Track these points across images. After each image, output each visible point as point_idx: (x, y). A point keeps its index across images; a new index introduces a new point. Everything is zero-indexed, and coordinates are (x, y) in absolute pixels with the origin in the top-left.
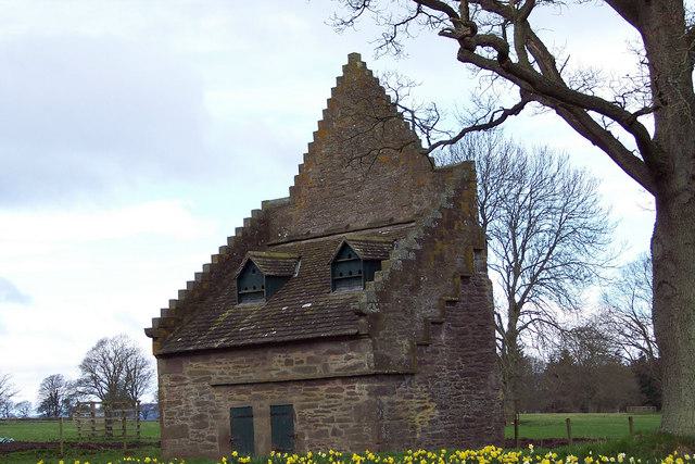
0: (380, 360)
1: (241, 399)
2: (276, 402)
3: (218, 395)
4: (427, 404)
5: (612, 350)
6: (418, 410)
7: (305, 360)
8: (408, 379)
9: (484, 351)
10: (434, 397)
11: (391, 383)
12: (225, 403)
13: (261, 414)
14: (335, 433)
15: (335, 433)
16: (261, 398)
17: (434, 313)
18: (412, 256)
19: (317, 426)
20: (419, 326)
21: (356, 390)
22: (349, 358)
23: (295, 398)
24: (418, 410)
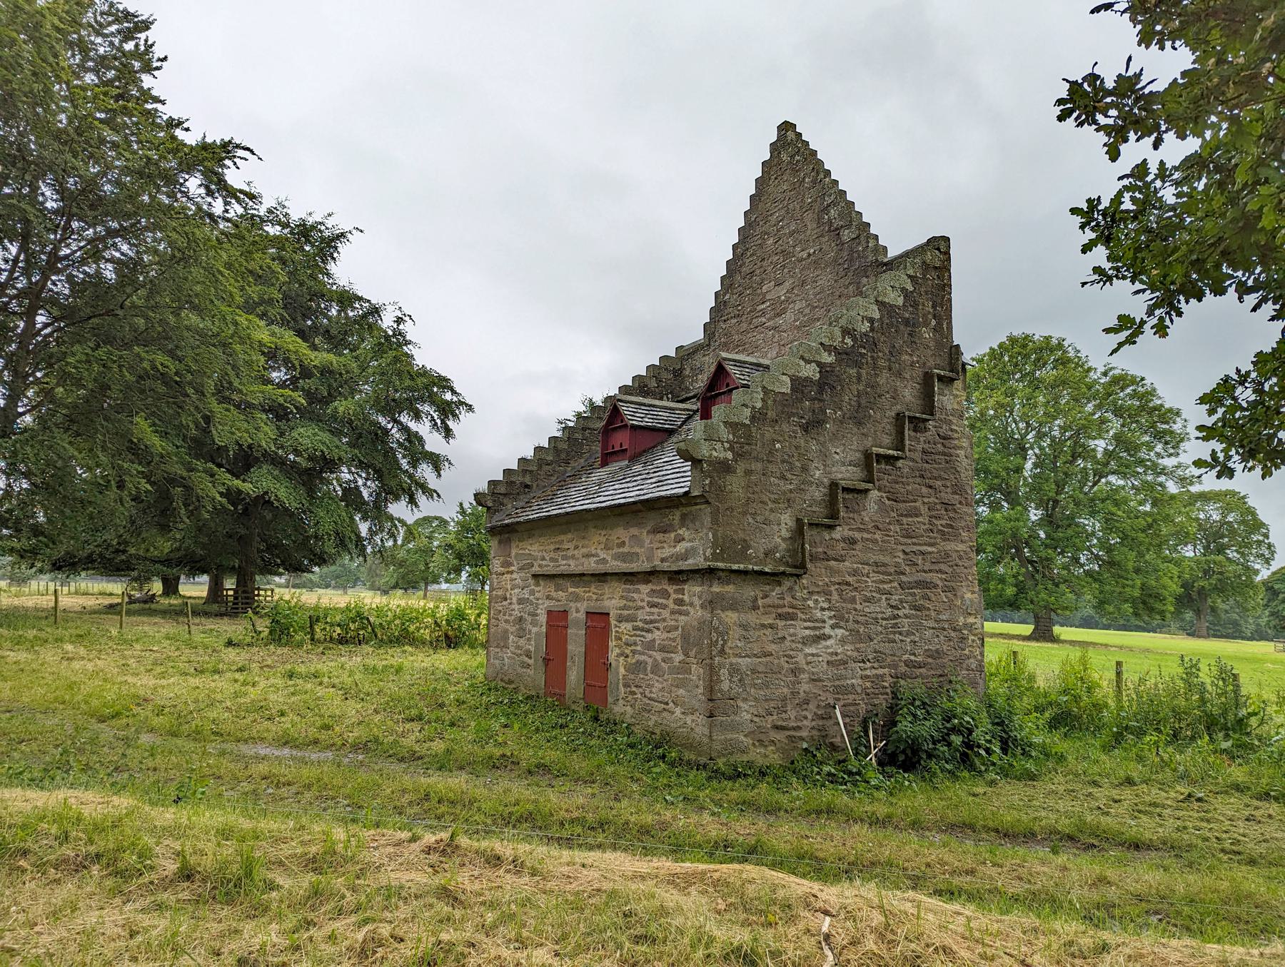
0: (724, 547)
1: (561, 596)
2: (594, 606)
3: (542, 590)
4: (827, 631)
5: (858, 882)
6: (806, 641)
7: (627, 540)
8: (787, 583)
9: (950, 546)
10: (842, 618)
11: (749, 591)
12: (544, 599)
13: (577, 621)
14: (656, 666)
15: (656, 669)
16: (577, 598)
17: (847, 474)
18: (811, 371)
19: (634, 652)
20: (818, 494)
21: (686, 598)
22: (680, 539)
23: (612, 599)
24: (806, 641)
